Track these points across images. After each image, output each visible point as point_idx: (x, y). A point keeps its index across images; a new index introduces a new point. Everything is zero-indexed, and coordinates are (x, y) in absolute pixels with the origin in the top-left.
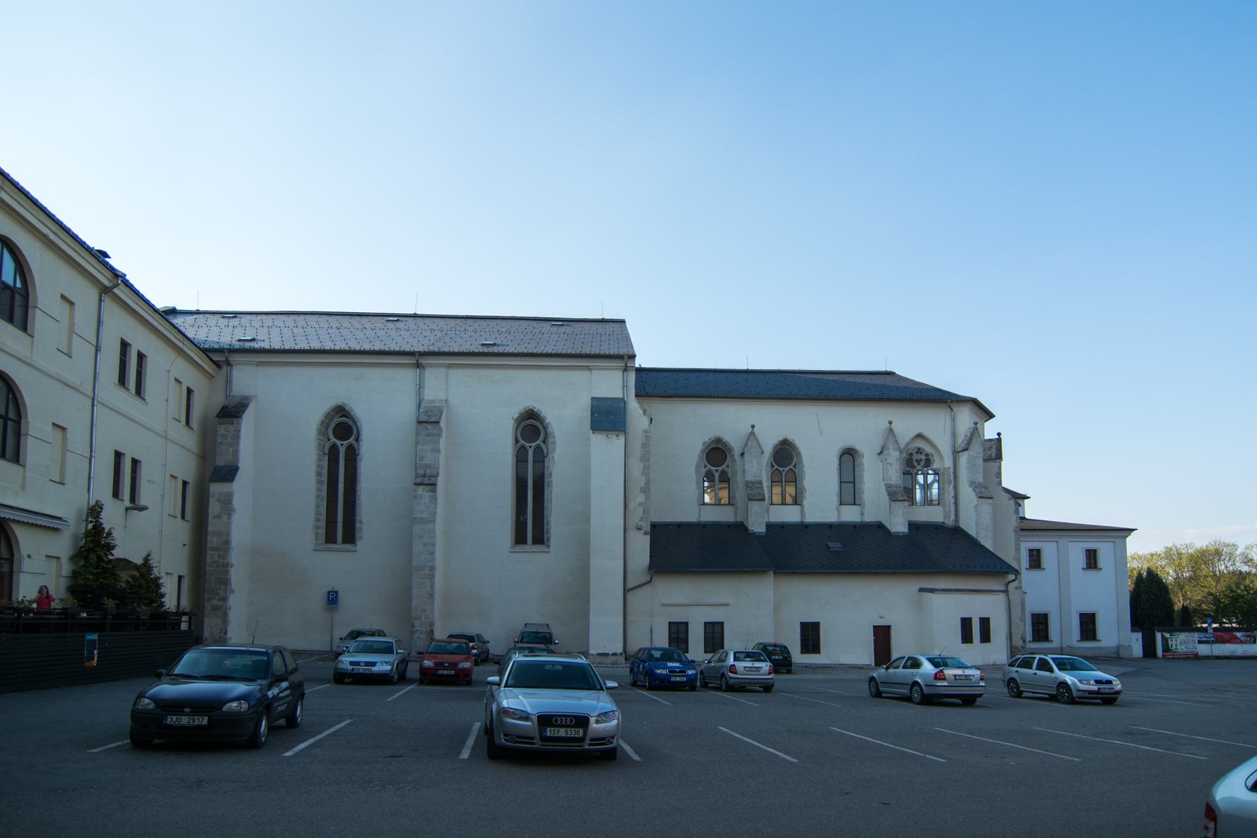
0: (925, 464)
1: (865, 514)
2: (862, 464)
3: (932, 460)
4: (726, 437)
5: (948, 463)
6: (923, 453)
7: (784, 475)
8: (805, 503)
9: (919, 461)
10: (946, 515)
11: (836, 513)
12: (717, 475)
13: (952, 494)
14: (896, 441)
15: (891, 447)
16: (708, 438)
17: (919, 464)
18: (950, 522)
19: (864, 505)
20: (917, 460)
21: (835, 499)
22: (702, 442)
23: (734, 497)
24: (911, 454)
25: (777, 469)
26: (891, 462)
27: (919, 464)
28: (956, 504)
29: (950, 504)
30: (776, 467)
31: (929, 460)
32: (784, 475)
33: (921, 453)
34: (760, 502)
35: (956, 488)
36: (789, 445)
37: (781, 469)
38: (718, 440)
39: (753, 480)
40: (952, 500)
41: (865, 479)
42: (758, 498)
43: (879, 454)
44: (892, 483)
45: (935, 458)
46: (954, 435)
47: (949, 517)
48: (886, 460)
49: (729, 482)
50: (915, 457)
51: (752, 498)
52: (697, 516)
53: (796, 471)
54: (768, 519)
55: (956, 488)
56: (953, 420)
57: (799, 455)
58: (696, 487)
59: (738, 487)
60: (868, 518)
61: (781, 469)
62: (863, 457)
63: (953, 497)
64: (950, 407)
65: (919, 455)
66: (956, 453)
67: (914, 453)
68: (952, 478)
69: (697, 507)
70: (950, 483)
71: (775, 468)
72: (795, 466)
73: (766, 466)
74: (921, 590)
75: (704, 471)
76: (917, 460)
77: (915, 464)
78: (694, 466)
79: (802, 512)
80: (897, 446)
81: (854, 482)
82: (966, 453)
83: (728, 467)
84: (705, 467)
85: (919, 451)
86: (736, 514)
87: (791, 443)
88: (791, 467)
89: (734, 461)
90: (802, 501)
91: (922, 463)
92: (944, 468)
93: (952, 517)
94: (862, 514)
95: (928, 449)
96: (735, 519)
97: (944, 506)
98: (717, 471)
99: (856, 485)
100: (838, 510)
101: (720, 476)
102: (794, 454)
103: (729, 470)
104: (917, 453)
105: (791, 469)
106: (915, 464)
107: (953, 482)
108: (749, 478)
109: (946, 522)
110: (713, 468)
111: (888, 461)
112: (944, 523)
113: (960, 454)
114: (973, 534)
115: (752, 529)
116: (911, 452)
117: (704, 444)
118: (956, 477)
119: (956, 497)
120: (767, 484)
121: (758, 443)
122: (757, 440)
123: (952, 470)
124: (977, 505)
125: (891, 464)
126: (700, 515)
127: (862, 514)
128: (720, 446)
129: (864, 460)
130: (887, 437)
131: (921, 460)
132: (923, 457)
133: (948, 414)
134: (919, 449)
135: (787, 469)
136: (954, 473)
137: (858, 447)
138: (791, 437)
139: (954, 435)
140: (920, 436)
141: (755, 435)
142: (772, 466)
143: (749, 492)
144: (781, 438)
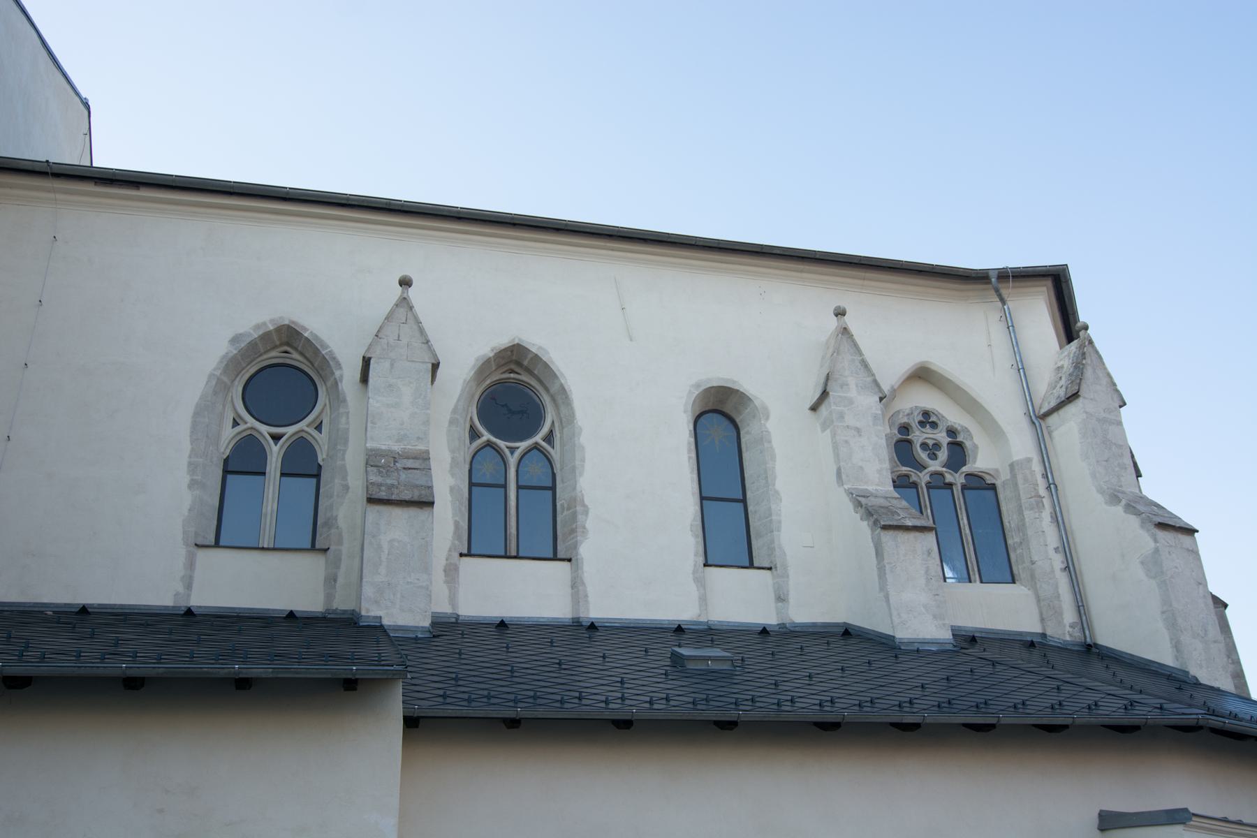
0: (950, 457)
1: (792, 599)
2: (764, 439)
3: (968, 444)
4: (315, 325)
5: (1021, 444)
6: (940, 427)
7: (512, 461)
8: (586, 550)
9: (933, 450)
10: (1047, 607)
11: (693, 591)
12: (275, 453)
13: (1052, 539)
14: (865, 364)
15: (852, 382)
16: (254, 323)
17: (933, 457)
18: (1064, 629)
19: (785, 567)
20: (924, 446)
21: (688, 543)
22: (230, 334)
23: (330, 523)
24: (905, 429)
25: (489, 444)
26: (858, 425)
27: (933, 457)
28: (1070, 568)
29: (1053, 571)
30: (487, 436)
31: (959, 445)
32: (512, 461)
33: (934, 425)
34: (413, 512)
35: (1058, 520)
36: (529, 371)
37: (502, 444)
38: (289, 336)
39: (397, 448)
40: (1058, 561)
41: (780, 484)
42: (407, 495)
43: (814, 408)
44: (871, 488)
45: (976, 440)
46: (1021, 369)
47: (1059, 613)
48: (841, 416)
49: (317, 476)
50: (919, 436)
51: (383, 495)
52: (180, 588)
53: (555, 454)
54: (453, 600)
55: (1058, 520)
56: (1011, 328)
57: (562, 397)
58: (186, 479)
59: (346, 488)
60: (803, 612)
61: (502, 444)
62: (767, 418)
63: (1056, 550)
64: (997, 291)
65: (928, 428)
66: (1039, 419)
67: (915, 425)
68: (1042, 491)
69: (182, 551)
70: (1039, 505)
71: (484, 439)
72: (549, 438)
73: (452, 422)
74: (1108, 821)
75: (228, 436)
76: (924, 446)
77: (923, 456)
78: (190, 410)
79: (576, 584)
80: (869, 379)
81: (744, 501)
82: (1072, 409)
83: (319, 428)
84: (235, 424)
85: (928, 419)
86: (331, 581)
87: (536, 358)
88: (538, 438)
89: (337, 398)
90: (575, 547)
91: (943, 455)
92: (1012, 466)
93: (1069, 616)
94: (781, 598)
95: (951, 414)
96: (329, 597)
97: (1033, 581)
98: (277, 438)
99: (750, 508)
100: (700, 582)
101: (287, 457)
102: (546, 399)
103: (322, 442)
104: (922, 424)
105: (536, 447)
106: (923, 456)
107: (1047, 502)
108: (383, 440)
109: (1049, 633)
110: (265, 429)
111: (850, 420)
112: (1044, 635)
113: (1053, 419)
114: (1164, 656)
115: (375, 612)
116: (905, 420)
117: (235, 340)
118: (1052, 487)
119: (1066, 549)
120: (451, 481)
121: (422, 331)
122: (418, 322)
123: (1037, 468)
124: (1157, 550)
125: (858, 430)
126: (189, 586)
127: (781, 598)
128: (295, 358)
129: (772, 425)
130: (837, 351)
131: (937, 446)
132: (944, 439)
133: (994, 316)
134: (926, 414)
135: (523, 445)
136: (1045, 476)
137: (746, 385)
138: (535, 340)
139: (1021, 369)
140: (923, 375)
141: (411, 308)
142: (474, 434)
143: (374, 478)
144: (503, 341)
